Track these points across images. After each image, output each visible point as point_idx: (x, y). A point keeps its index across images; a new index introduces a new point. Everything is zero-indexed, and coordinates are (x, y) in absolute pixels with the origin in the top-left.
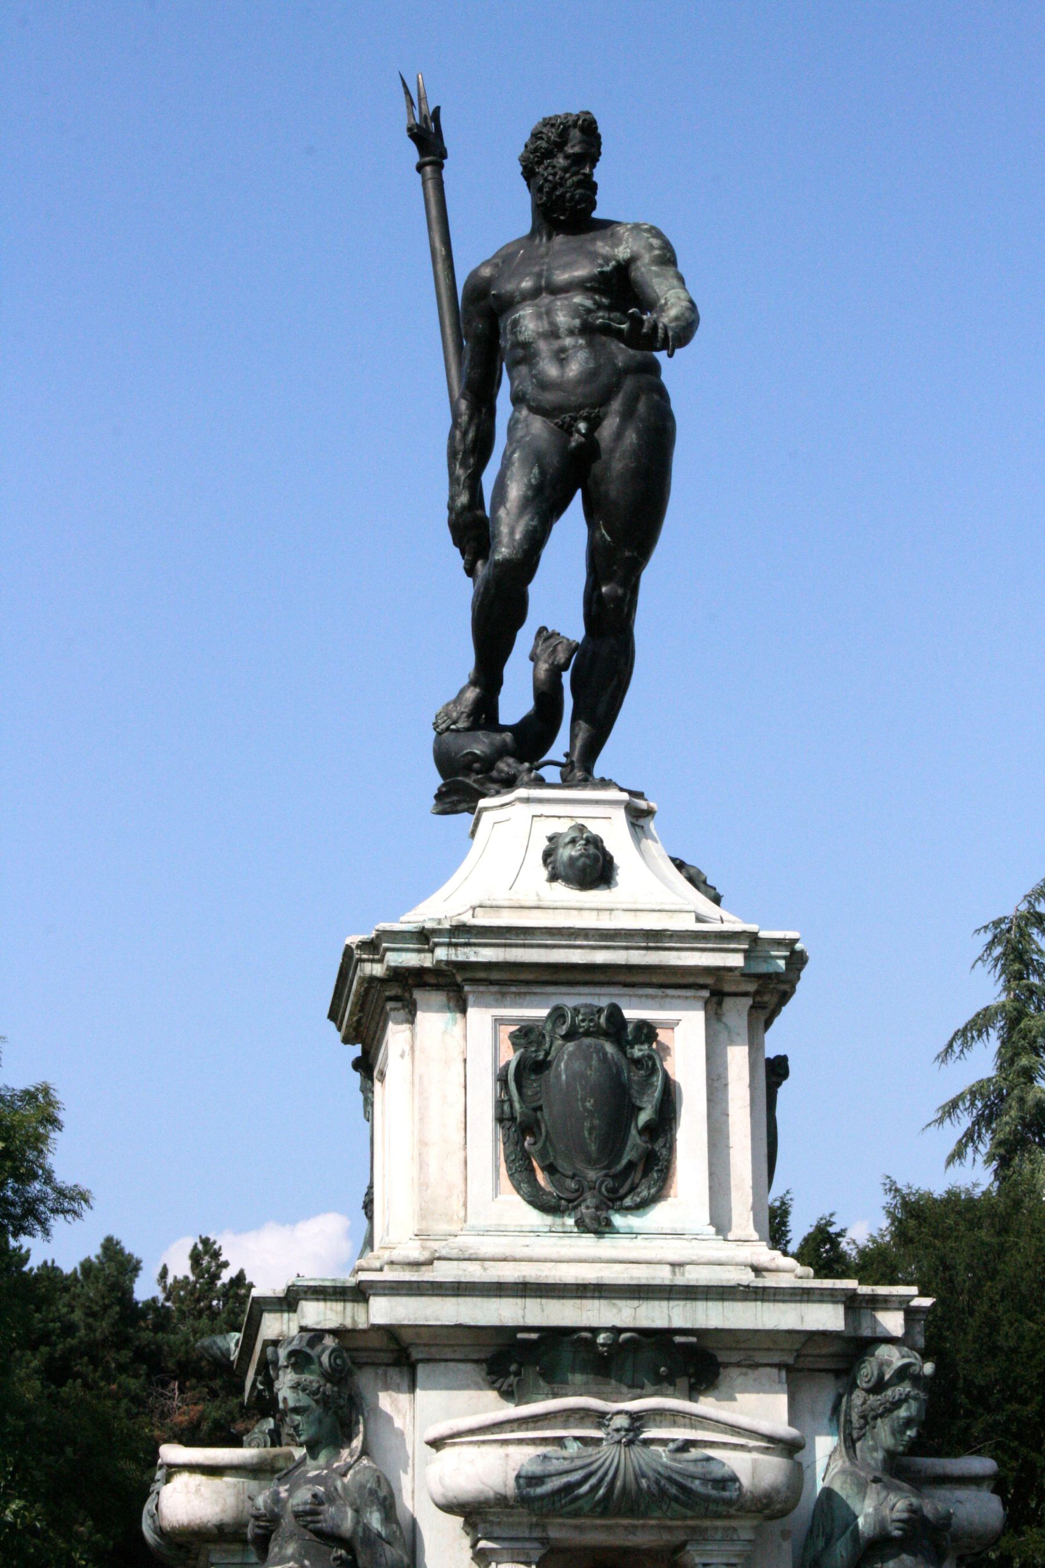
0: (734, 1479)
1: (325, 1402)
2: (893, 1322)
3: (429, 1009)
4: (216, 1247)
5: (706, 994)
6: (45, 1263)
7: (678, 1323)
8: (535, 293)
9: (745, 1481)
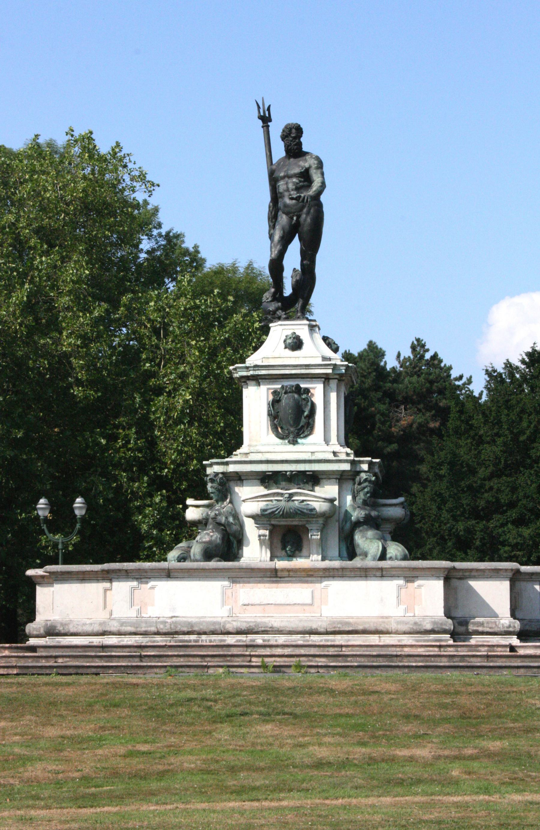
0: (315, 509)
1: (219, 491)
2: (365, 467)
3: (251, 386)
4: (423, 342)
5: (323, 380)
6: (346, 351)
7: (307, 469)
8: (283, 178)
9: (318, 509)
